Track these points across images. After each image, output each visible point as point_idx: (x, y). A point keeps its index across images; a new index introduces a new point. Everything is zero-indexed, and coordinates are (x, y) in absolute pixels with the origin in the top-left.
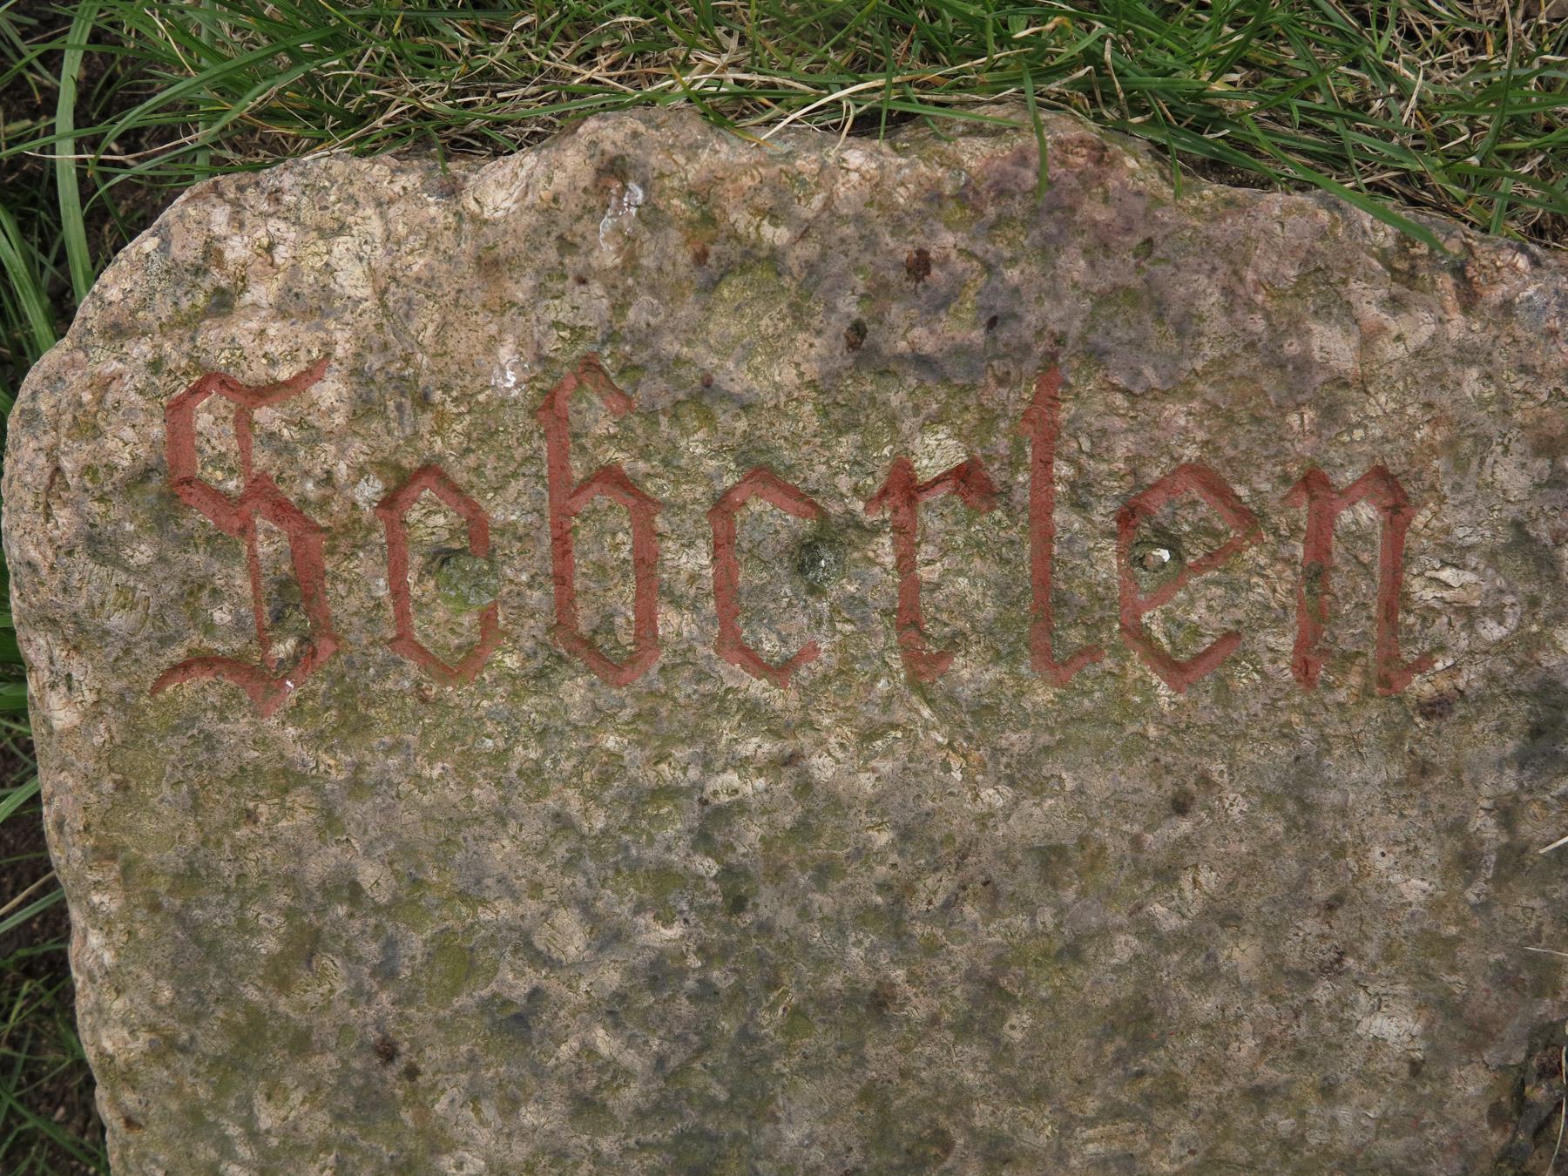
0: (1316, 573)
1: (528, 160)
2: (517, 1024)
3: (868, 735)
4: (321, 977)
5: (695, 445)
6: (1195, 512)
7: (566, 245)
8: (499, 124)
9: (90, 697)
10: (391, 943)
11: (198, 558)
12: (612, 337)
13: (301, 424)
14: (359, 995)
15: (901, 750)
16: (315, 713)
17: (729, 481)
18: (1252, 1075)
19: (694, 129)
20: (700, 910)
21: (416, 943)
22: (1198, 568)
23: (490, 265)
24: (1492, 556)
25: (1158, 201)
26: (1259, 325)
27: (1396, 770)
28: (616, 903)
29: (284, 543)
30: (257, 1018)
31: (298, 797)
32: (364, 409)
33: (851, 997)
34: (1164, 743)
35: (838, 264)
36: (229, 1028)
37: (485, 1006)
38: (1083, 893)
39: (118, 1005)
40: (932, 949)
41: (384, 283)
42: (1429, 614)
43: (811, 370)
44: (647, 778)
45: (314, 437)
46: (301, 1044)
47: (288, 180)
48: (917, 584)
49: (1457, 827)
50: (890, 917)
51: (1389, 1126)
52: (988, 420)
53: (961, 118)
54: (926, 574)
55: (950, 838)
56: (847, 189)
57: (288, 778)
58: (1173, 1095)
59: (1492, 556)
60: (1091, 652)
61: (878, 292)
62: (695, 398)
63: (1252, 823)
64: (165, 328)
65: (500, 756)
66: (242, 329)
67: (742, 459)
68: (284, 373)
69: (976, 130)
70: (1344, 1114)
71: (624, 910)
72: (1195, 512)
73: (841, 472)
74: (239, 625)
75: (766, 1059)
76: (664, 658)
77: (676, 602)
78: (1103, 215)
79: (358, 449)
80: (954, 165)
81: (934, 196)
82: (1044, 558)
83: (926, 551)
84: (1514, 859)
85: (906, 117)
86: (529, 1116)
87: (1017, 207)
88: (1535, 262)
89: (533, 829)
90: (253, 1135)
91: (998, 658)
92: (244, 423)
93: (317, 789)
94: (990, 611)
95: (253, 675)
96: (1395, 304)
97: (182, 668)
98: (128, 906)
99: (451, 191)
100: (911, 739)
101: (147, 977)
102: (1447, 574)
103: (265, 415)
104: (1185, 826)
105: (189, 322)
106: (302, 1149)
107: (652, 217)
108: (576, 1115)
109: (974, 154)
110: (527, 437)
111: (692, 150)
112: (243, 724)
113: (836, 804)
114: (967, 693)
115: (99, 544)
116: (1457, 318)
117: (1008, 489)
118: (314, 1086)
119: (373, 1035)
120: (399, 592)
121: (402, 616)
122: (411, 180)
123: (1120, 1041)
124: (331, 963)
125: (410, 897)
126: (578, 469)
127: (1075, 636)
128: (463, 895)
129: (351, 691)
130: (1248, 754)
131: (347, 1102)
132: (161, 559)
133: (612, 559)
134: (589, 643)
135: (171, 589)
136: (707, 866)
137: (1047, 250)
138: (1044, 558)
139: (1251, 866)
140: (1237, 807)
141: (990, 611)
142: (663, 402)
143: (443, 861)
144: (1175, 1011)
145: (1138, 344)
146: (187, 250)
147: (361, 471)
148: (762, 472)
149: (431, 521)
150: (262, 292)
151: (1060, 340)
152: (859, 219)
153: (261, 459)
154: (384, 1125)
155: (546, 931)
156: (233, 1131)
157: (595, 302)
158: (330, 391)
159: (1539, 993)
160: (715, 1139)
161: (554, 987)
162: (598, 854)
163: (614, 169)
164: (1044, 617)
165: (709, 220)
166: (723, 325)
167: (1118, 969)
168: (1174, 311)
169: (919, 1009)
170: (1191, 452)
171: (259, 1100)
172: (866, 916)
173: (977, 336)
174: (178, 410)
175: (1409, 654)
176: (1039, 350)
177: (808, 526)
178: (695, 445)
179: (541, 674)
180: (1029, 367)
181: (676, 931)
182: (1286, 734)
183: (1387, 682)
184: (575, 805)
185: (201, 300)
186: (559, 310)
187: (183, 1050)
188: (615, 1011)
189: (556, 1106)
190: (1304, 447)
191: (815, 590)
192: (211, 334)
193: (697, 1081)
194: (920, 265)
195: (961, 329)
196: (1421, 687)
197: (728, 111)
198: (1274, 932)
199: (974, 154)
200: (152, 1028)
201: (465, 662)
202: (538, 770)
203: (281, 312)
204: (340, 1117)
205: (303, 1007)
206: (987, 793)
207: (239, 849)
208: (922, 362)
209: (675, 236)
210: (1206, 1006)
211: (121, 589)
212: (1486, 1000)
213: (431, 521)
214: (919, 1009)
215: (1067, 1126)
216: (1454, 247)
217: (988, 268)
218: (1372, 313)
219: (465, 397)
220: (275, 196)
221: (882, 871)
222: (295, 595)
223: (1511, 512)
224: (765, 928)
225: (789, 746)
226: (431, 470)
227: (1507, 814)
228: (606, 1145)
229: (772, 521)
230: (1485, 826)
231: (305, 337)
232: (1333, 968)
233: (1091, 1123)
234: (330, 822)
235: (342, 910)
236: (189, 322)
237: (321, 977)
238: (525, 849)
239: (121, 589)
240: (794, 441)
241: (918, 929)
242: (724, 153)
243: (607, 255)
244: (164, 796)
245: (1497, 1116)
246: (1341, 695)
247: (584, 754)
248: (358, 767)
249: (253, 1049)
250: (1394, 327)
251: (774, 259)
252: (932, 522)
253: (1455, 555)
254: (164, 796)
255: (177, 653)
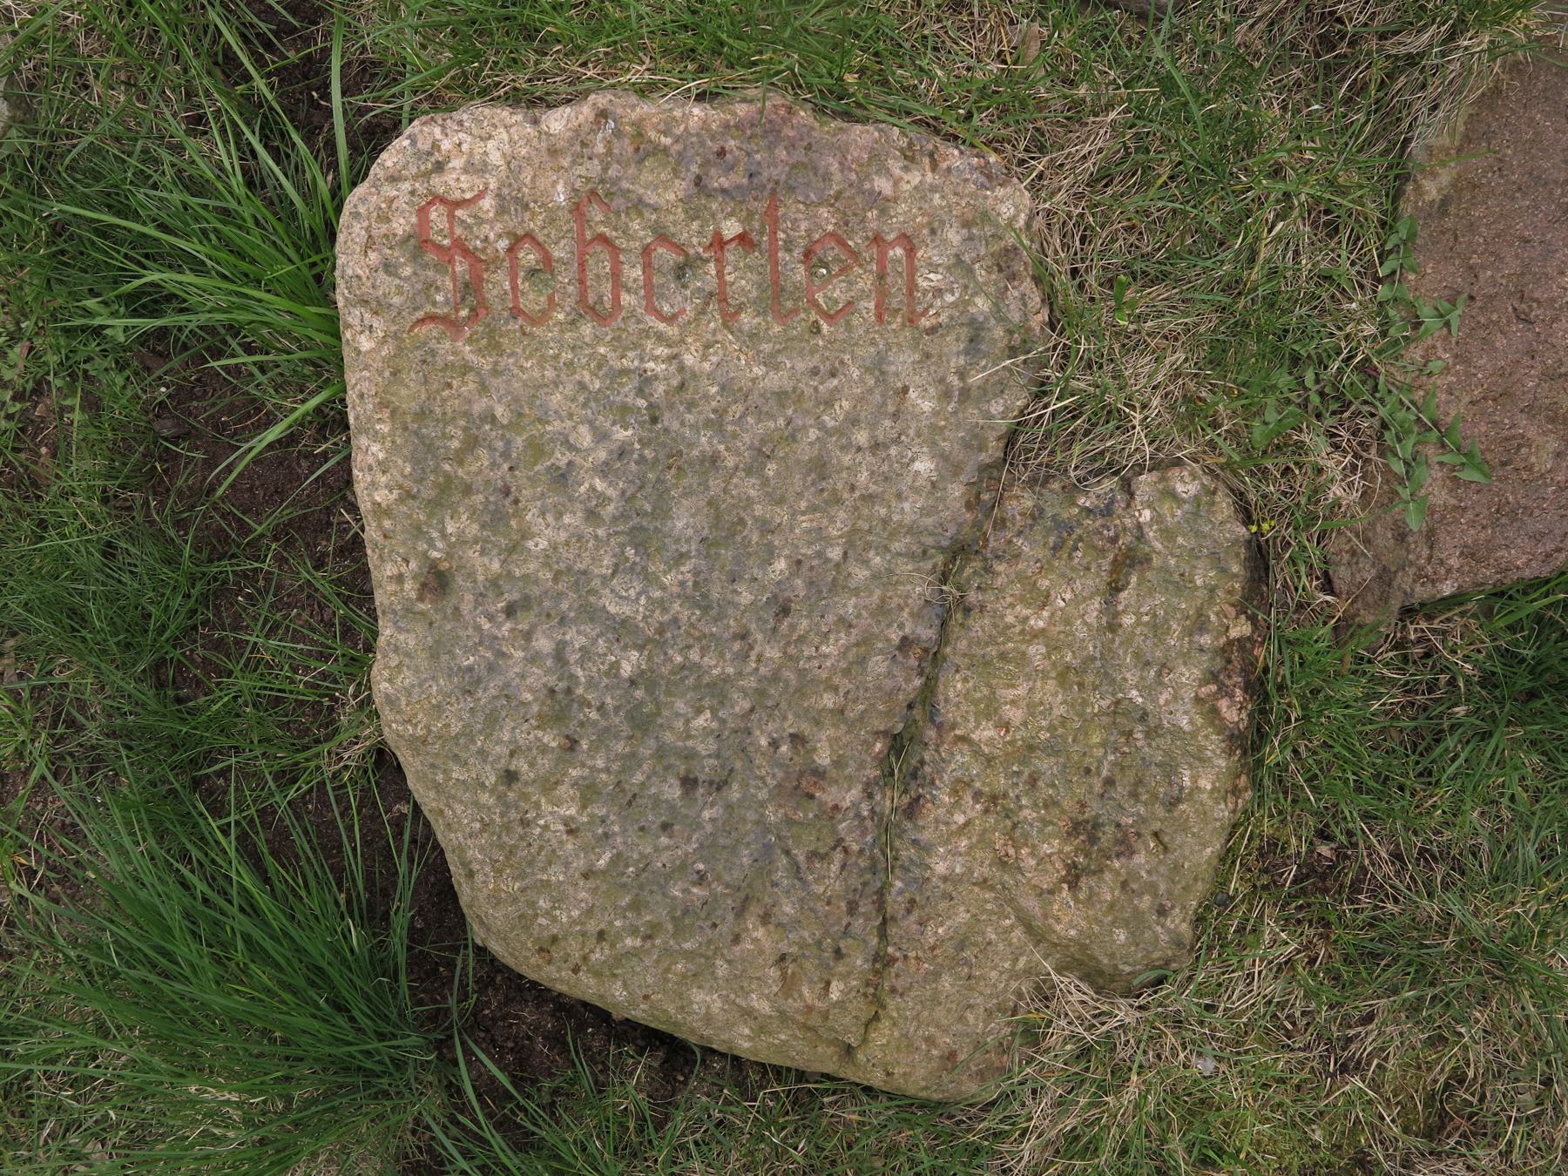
0: (881, 276)
1: (567, 110)
2: (562, 478)
3: (707, 346)
4: (478, 459)
5: (635, 225)
6: (832, 252)
7: (584, 145)
8: (547, 94)
9: (381, 334)
10: (508, 443)
11: (430, 273)
12: (602, 181)
13: (475, 217)
14: (494, 465)
15: (721, 352)
16: (477, 341)
17: (649, 240)
18: (867, 488)
19: (634, 99)
20: (639, 423)
21: (519, 442)
22: (836, 276)
23: (553, 152)
24: (948, 268)
25: (812, 128)
26: (853, 176)
27: (917, 357)
28: (604, 422)
29: (466, 267)
30: (448, 478)
31: (470, 377)
32: (502, 210)
33: (702, 459)
34: (825, 348)
35: (690, 153)
36: (436, 485)
37: (548, 469)
38: (795, 411)
39: (384, 479)
40: (735, 436)
41: (509, 160)
42: (925, 292)
43: (681, 195)
44: (617, 365)
45: (480, 221)
46: (468, 490)
47: (465, 117)
48: (725, 283)
49: (942, 381)
50: (716, 424)
51: (926, 512)
52: (751, 215)
53: (738, 95)
54: (728, 278)
55: (741, 389)
56: (693, 123)
57: (466, 369)
58: (837, 500)
59: (948, 268)
60: (795, 311)
61: (706, 164)
62: (635, 206)
63: (861, 380)
64: (415, 178)
65: (556, 357)
66: (450, 178)
67: (654, 231)
68: (468, 196)
69: (744, 100)
70: (907, 506)
71: (608, 424)
72: (832, 252)
73: (693, 237)
74: (447, 302)
75: (667, 490)
76: (624, 314)
77: (628, 291)
78: (791, 134)
79: (498, 227)
80: (734, 114)
81: (727, 126)
82: (775, 272)
83: (729, 269)
84: (965, 393)
85: (718, 94)
86: (567, 519)
87: (758, 130)
88: (961, 153)
89: (569, 389)
90: (444, 536)
91: (758, 314)
92: (451, 216)
93: (478, 373)
94: (755, 293)
95: (451, 324)
96: (906, 169)
97: (422, 321)
98: (393, 429)
99: (535, 122)
100: (724, 348)
101: (400, 462)
102: (931, 276)
103: (459, 213)
104: (835, 382)
105: (427, 175)
106: (465, 542)
107: (618, 133)
108: (587, 519)
109: (742, 110)
110: (568, 222)
111: (633, 107)
112: (447, 345)
113: (694, 376)
114: (746, 328)
115: (389, 267)
116: (930, 174)
117: (759, 244)
118: (473, 512)
119: (500, 483)
120: (514, 287)
121: (516, 297)
122: (519, 117)
123: (813, 475)
124: (482, 452)
125: (515, 425)
126: (589, 235)
127: (789, 304)
128: (540, 420)
129: (493, 331)
130: (859, 352)
131: (487, 518)
132: (415, 273)
133: (602, 273)
134: (593, 309)
135: (419, 286)
136: (642, 403)
137: (771, 148)
138: (775, 272)
139: (861, 399)
140: (856, 374)
141: (755, 293)
142: (623, 207)
143: (531, 405)
144: (835, 461)
145: (808, 185)
146: (424, 145)
147: (500, 236)
148: (663, 237)
149: (528, 257)
150: (457, 163)
151: (777, 183)
152: (698, 135)
153: (458, 231)
154: (502, 529)
155: (575, 435)
156: (435, 535)
157: (594, 168)
158: (487, 203)
159: (980, 450)
160: (647, 530)
161: (578, 460)
162: (596, 400)
163: (603, 114)
164: (775, 297)
165: (640, 135)
166: (646, 176)
167: (811, 444)
168: (821, 172)
169: (730, 462)
170: (830, 228)
171: (448, 518)
172: (708, 424)
173: (745, 181)
174: (422, 212)
175: (919, 309)
176: (769, 186)
177: (681, 259)
178: (635, 225)
179: (573, 322)
180: (766, 194)
181: (630, 432)
182: (873, 343)
183: (911, 320)
184: (587, 377)
185: (429, 166)
186: (581, 170)
187: (414, 497)
188: (604, 470)
189: (579, 514)
190: (873, 225)
191: (684, 286)
192: (436, 180)
193: (638, 504)
194: (722, 153)
195: (739, 178)
196: (925, 323)
197: (644, 91)
198: (873, 426)
199: (742, 110)
200: (401, 487)
201: (541, 318)
202: (572, 363)
203: (465, 171)
204: (483, 527)
205: (468, 473)
206: (755, 369)
207: (444, 401)
208: (724, 191)
209: (627, 141)
210: (846, 459)
211: (398, 287)
212: (959, 454)
213: (528, 257)
214: (730, 462)
215: (793, 515)
216: (930, 147)
217: (748, 154)
218: (897, 172)
219: (543, 205)
220: (461, 123)
221: (714, 403)
222: (471, 289)
223: (954, 251)
224: (666, 430)
225: (675, 350)
226: (529, 236)
227: (962, 375)
228: (601, 532)
229: (666, 256)
230: (954, 380)
231: (477, 181)
232: (897, 441)
233: (803, 513)
234: (483, 388)
235: (487, 427)
236: (427, 175)
237: (478, 459)
238: (566, 397)
239: (398, 287)
240: (675, 223)
241: (729, 428)
242: (645, 109)
243: (600, 148)
244: (411, 377)
245: (969, 506)
246: (894, 326)
247: (590, 355)
248: (496, 363)
249: (446, 494)
250: (906, 178)
251: (666, 150)
252: (730, 257)
253: (934, 268)
254: (411, 377)
255: (420, 314)
